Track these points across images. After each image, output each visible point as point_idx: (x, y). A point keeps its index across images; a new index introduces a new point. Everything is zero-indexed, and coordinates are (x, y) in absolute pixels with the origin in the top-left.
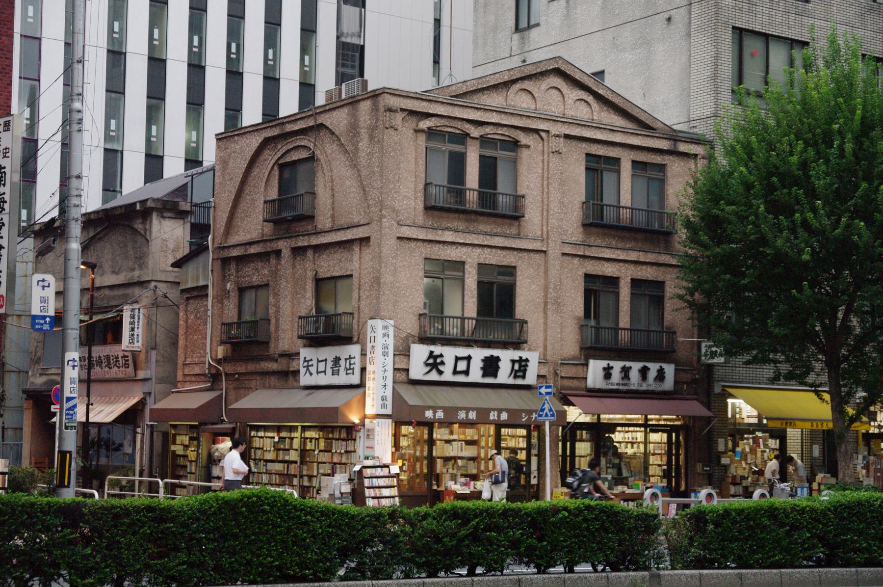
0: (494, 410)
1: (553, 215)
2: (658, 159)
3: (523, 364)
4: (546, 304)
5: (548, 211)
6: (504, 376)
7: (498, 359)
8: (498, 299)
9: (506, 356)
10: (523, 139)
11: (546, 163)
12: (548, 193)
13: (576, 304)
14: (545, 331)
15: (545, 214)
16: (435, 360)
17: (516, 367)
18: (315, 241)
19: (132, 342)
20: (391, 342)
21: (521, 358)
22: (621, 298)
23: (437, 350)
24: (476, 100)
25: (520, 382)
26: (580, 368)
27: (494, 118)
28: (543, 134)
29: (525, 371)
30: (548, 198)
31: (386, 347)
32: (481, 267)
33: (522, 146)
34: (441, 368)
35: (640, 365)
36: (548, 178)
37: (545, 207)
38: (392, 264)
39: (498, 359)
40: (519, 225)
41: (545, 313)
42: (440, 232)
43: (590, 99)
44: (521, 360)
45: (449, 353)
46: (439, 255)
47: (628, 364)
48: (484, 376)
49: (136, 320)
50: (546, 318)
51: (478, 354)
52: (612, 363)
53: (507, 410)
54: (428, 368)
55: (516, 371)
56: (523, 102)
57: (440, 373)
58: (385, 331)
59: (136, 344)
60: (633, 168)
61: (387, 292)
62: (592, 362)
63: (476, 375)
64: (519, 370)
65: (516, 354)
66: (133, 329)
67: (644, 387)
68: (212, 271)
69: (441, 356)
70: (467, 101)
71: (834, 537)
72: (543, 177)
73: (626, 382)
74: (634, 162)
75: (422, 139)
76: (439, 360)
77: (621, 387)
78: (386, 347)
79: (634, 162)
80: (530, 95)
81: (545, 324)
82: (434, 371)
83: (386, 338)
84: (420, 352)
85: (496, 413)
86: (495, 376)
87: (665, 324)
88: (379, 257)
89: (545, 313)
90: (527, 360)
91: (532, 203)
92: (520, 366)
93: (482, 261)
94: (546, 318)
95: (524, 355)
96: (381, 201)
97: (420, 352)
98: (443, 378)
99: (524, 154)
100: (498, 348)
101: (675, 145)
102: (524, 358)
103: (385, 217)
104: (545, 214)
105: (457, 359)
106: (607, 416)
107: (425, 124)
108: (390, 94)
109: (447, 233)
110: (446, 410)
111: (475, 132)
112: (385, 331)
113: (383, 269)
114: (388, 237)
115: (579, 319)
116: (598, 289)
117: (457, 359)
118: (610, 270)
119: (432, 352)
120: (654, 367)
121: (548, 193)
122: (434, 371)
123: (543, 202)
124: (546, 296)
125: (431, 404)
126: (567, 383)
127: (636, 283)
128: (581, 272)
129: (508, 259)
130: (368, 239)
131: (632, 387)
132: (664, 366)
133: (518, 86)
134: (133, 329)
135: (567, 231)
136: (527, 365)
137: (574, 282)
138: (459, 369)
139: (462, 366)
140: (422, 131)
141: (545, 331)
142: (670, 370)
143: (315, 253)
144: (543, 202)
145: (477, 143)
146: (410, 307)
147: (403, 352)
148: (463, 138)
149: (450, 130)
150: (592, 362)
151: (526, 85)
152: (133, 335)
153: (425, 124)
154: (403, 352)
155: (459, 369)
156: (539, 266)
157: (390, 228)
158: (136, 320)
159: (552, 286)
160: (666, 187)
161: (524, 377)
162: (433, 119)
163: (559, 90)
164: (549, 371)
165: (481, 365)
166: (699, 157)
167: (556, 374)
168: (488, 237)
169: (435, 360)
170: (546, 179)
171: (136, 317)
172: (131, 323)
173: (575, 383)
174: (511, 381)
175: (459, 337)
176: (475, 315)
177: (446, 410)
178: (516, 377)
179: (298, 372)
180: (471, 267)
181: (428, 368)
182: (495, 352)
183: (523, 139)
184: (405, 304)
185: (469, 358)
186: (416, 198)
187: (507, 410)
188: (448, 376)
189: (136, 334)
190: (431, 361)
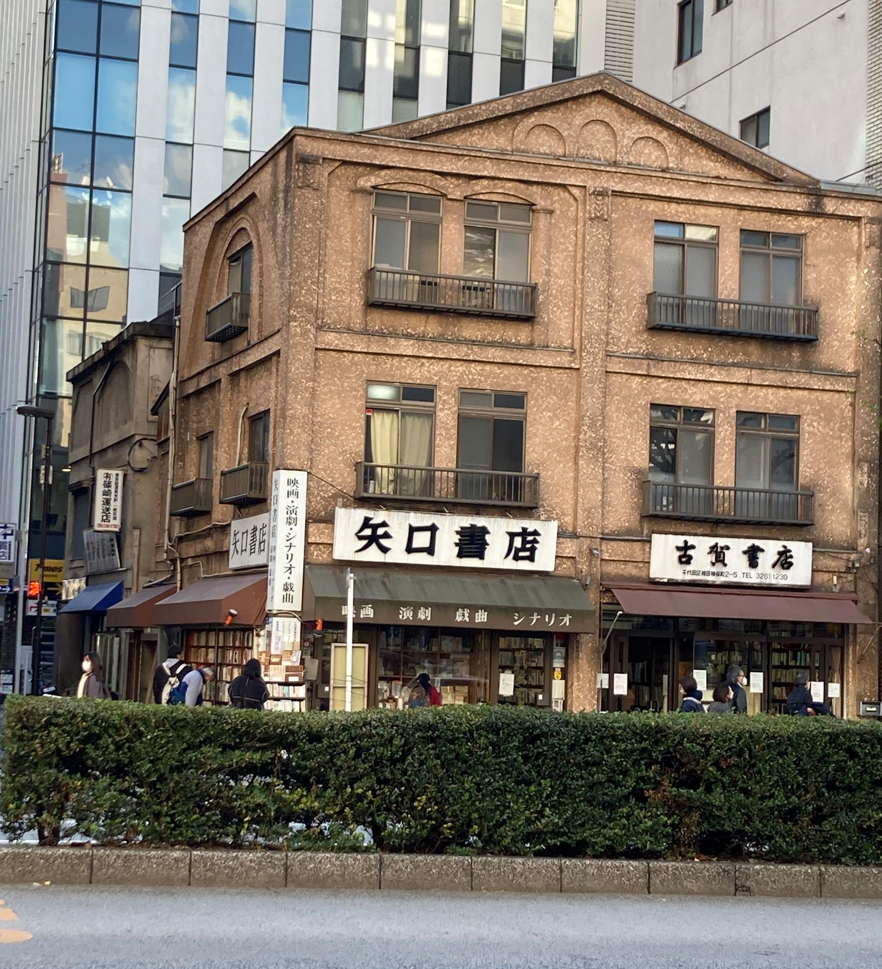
0: (464, 607)
1: (591, 314)
2: (789, 225)
3: (530, 538)
4: (577, 448)
5: (582, 308)
6: (496, 556)
7: (484, 531)
9: (499, 531)
10: (536, 195)
12: (582, 281)
13: (633, 449)
14: (576, 490)
15: (578, 313)
17: (518, 542)
20: (301, 504)
21: (524, 529)
22: (718, 442)
23: (379, 516)
25: (524, 565)
26: (637, 546)
27: (489, 170)
28: (576, 192)
29: (533, 550)
31: (292, 511)
32: (466, 394)
33: (538, 211)
34: (384, 542)
35: (747, 543)
36: (584, 258)
37: (579, 303)
38: (306, 389)
39: (484, 531)
40: (533, 329)
41: (576, 463)
42: (392, 341)
43: (663, 136)
44: (524, 533)
45: (398, 523)
47: (722, 542)
48: (460, 555)
49: (113, 489)
50: (577, 470)
51: (450, 527)
53: (571, 612)
55: (518, 550)
56: (543, 145)
57: (384, 550)
59: (112, 522)
60: (742, 242)
61: (297, 431)
63: (447, 553)
65: (516, 525)
68: (174, 416)
69: (384, 524)
70: (426, 145)
72: (575, 257)
73: (719, 568)
74: (746, 234)
75: (363, 206)
76: (380, 531)
77: (711, 579)
78: (292, 511)
79: (746, 234)
81: (576, 479)
82: (374, 546)
83: (292, 498)
84: (349, 520)
85: (467, 612)
87: (801, 481)
88: (286, 382)
89: (576, 463)
90: (536, 533)
91: (556, 297)
92: (524, 542)
93: (466, 384)
95: (531, 525)
96: (290, 296)
97: (349, 520)
98: (389, 558)
101: (818, 204)
102: (530, 530)
103: (294, 319)
104: (578, 313)
105: (412, 530)
107: (369, 181)
108: (307, 136)
109: (404, 342)
110: (437, 607)
111: (455, 189)
112: (290, 488)
114: (299, 348)
116: (674, 431)
117: (412, 530)
121: (582, 281)
122: (374, 546)
123: (575, 295)
124: (577, 438)
125: (537, 605)
126: (611, 569)
127: (746, 419)
128: (644, 401)
129: (510, 380)
130: (277, 353)
131: (731, 579)
133: (532, 120)
134: (108, 502)
135: (619, 339)
136: (535, 541)
137: (630, 416)
138: (415, 545)
139: (422, 540)
140: (363, 191)
141: (576, 490)
144: (575, 295)
145: (462, 208)
146: (340, 454)
147: (321, 518)
148: (431, 202)
149: (412, 189)
151: (547, 117)
152: (108, 509)
153: (369, 181)
154: (321, 518)
155: (415, 545)
156: (567, 392)
158: (113, 489)
159: (587, 421)
161: (531, 558)
162: (383, 173)
164: (580, 552)
166: (864, 221)
168: (476, 348)
170: (581, 262)
172: (105, 493)
173: (631, 570)
178: (516, 558)
179: (228, 552)
180: (446, 393)
182: (480, 521)
183: (536, 195)
184: (332, 448)
185: (433, 529)
186: (352, 292)
189: (112, 508)
190: (368, 532)
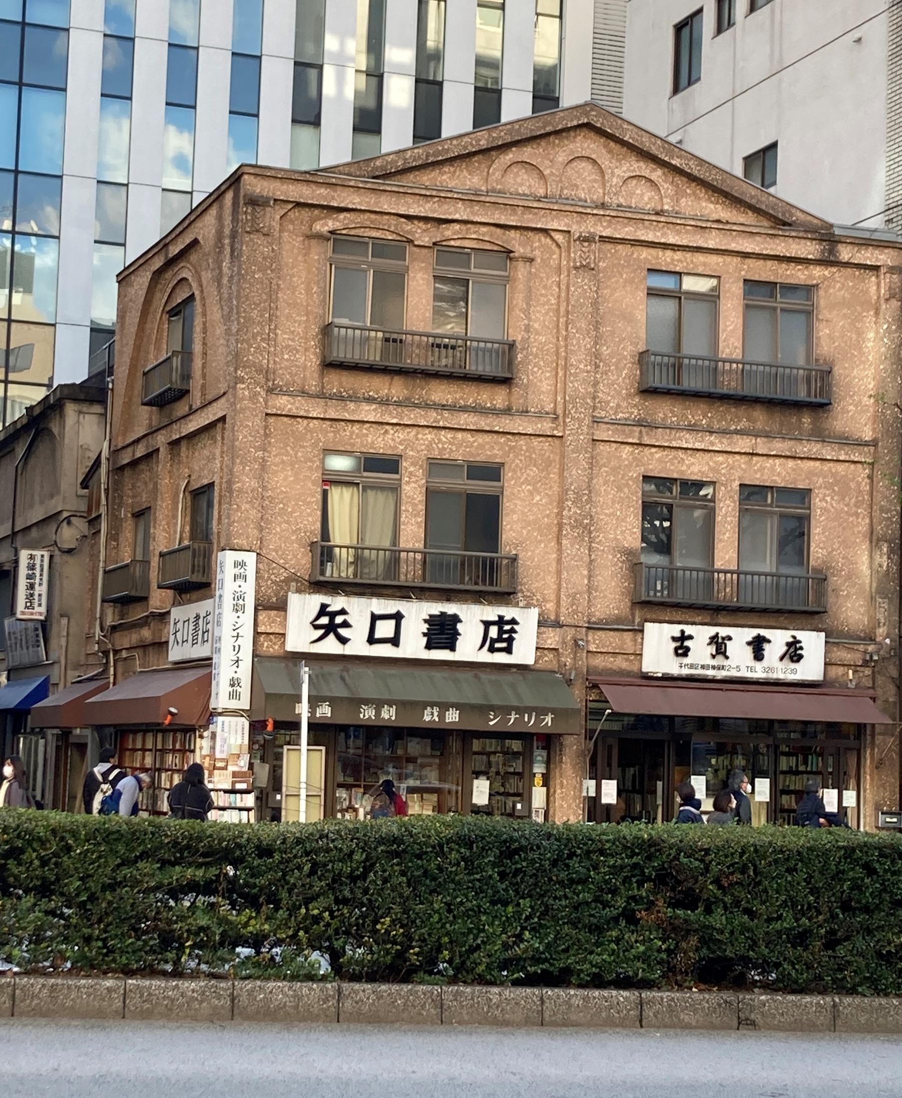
0: (432, 705)
2: (798, 275)
3: (507, 627)
4: (560, 526)
5: (565, 368)
7: (456, 619)
8: (471, 518)
9: (472, 619)
11: (563, 287)
13: (625, 528)
14: (559, 573)
15: (561, 373)
16: (332, 620)
17: (494, 632)
18: (193, 425)
19: (30, 605)
20: (249, 589)
23: (337, 603)
24: (426, 178)
25: (501, 658)
27: (460, 212)
28: (558, 237)
29: (510, 641)
30: (566, 346)
31: (239, 597)
32: (435, 466)
34: (343, 632)
35: (750, 633)
36: (567, 312)
40: (510, 392)
41: (559, 543)
42: (352, 406)
43: (657, 174)
44: (500, 621)
45: (358, 610)
46: (353, 445)
50: (560, 550)
51: (417, 614)
52: (689, 630)
53: (553, 711)
54: (321, 632)
55: (493, 641)
56: (522, 185)
57: (343, 641)
58: (237, 571)
59: (37, 609)
60: (747, 294)
62: (650, 628)
63: (413, 645)
64: (500, 639)
65: (491, 613)
66: (31, 586)
67: (759, 672)
69: (343, 612)
70: (391, 185)
71: (667, 862)
73: (719, 661)
75: (319, 253)
76: (339, 620)
77: (711, 673)
80: (535, 174)
81: (559, 561)
82: (332, 636)
83: (240, 582)
84: (303, 607)
86: (452, 648)
87: (812, 563)
88: (232, 452)
89: (559, 543)
90: (513, 622)
92: (501, 631)
94: (560, 550)
95: (509, 613)
96: (237, 354)
97: (303, 607)
98: (348, 650)
99: (521, 271)
100: (465, 601)
103: (242, 380)
104: (561, 373)
106: (306, 678)
109: (365, 407)
110: (403, 705)
111: (423, 235)
112: (237, 571)
113: (237, 468)
114: (248, 413)
115: (629, 553)
116: (669, 506)
118: (695, 469)
119: (324, 607)
120: (778, 639)
121: (566, 338)
122: (332, 636)
123: (557, 353)
124: (560, 514)
129: (485, 450)
130: (223, 419)
131: (734, 673)
132: (800, 635)
133: (510, 156)
134: (31, 586)
135: (608, 402)
137: (620, 489)
140: (319, 237)
141: (559, 573)
142: (813, 643)
143: (188, 444)
144: (557, 353)
146: (294, 532)
147: (271, 604)
148: (397, 248)
149: (374, 234)
150: (650, 628)
151: (527, 153)
152: (32, 595)
154: (271, 604)
155: (378, 635)
156: (549, 463)
157: (254, 397)
160: (816, 324)
161: (508, 650)
162: (342, 216)
163: (594, 162)
164: (564, 642)
165: (425, 627)
166: (883, 270)
167: (576, 644)
168: (446, 414)
169: (332, 620)
170: (565, 315)
171: (38, 567)
172: (29, 577)
173: (620, 663)
174: (485, 657)
175: (351, 579)
176: (420, 545)
177: (403, 705)
178: (492, 650)
179: (167, 642)
181: (321, 632)
182: (451, 608)
184: (284, 526)
185: (398, 617)
186: (306, 350)
187: (553, 711)
188: (358, 646)
189: (36, 593)
190: (324, 620)
